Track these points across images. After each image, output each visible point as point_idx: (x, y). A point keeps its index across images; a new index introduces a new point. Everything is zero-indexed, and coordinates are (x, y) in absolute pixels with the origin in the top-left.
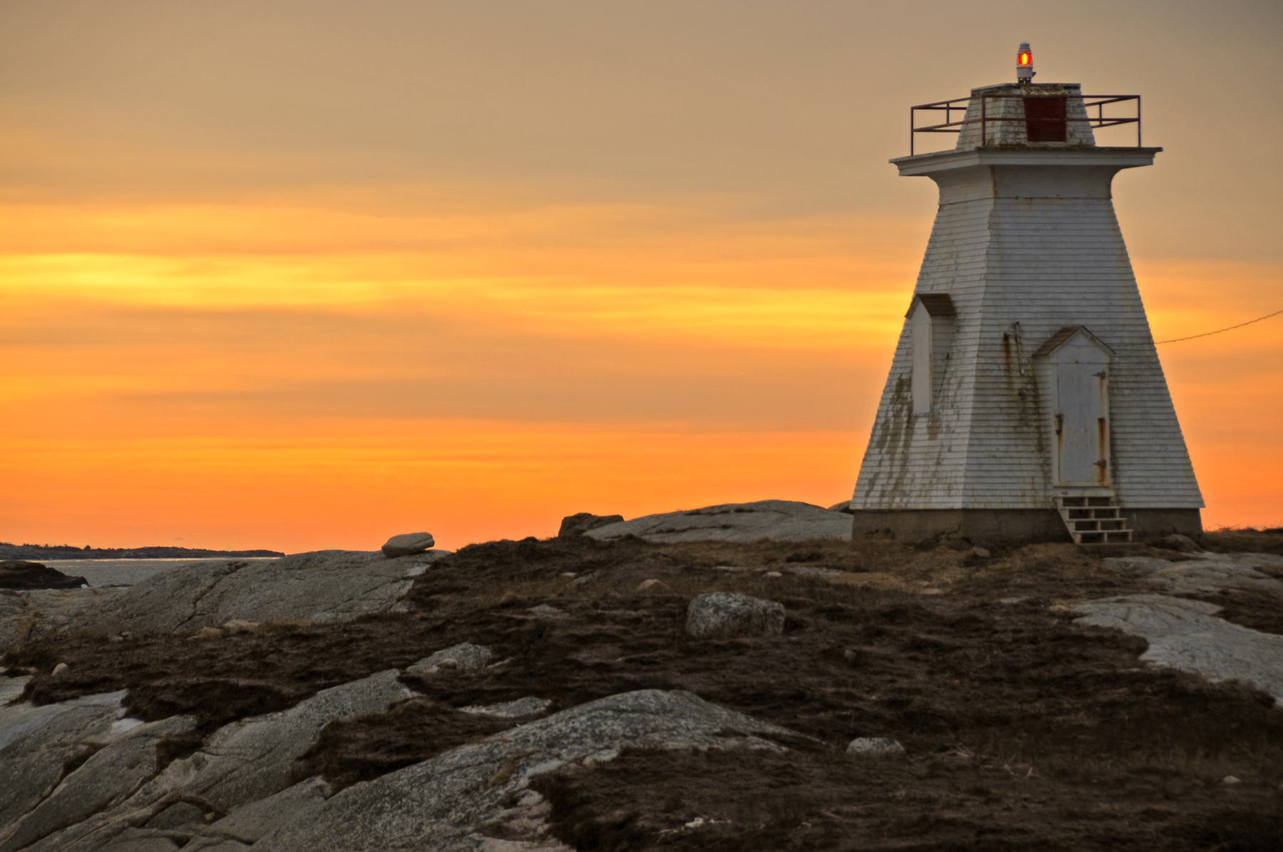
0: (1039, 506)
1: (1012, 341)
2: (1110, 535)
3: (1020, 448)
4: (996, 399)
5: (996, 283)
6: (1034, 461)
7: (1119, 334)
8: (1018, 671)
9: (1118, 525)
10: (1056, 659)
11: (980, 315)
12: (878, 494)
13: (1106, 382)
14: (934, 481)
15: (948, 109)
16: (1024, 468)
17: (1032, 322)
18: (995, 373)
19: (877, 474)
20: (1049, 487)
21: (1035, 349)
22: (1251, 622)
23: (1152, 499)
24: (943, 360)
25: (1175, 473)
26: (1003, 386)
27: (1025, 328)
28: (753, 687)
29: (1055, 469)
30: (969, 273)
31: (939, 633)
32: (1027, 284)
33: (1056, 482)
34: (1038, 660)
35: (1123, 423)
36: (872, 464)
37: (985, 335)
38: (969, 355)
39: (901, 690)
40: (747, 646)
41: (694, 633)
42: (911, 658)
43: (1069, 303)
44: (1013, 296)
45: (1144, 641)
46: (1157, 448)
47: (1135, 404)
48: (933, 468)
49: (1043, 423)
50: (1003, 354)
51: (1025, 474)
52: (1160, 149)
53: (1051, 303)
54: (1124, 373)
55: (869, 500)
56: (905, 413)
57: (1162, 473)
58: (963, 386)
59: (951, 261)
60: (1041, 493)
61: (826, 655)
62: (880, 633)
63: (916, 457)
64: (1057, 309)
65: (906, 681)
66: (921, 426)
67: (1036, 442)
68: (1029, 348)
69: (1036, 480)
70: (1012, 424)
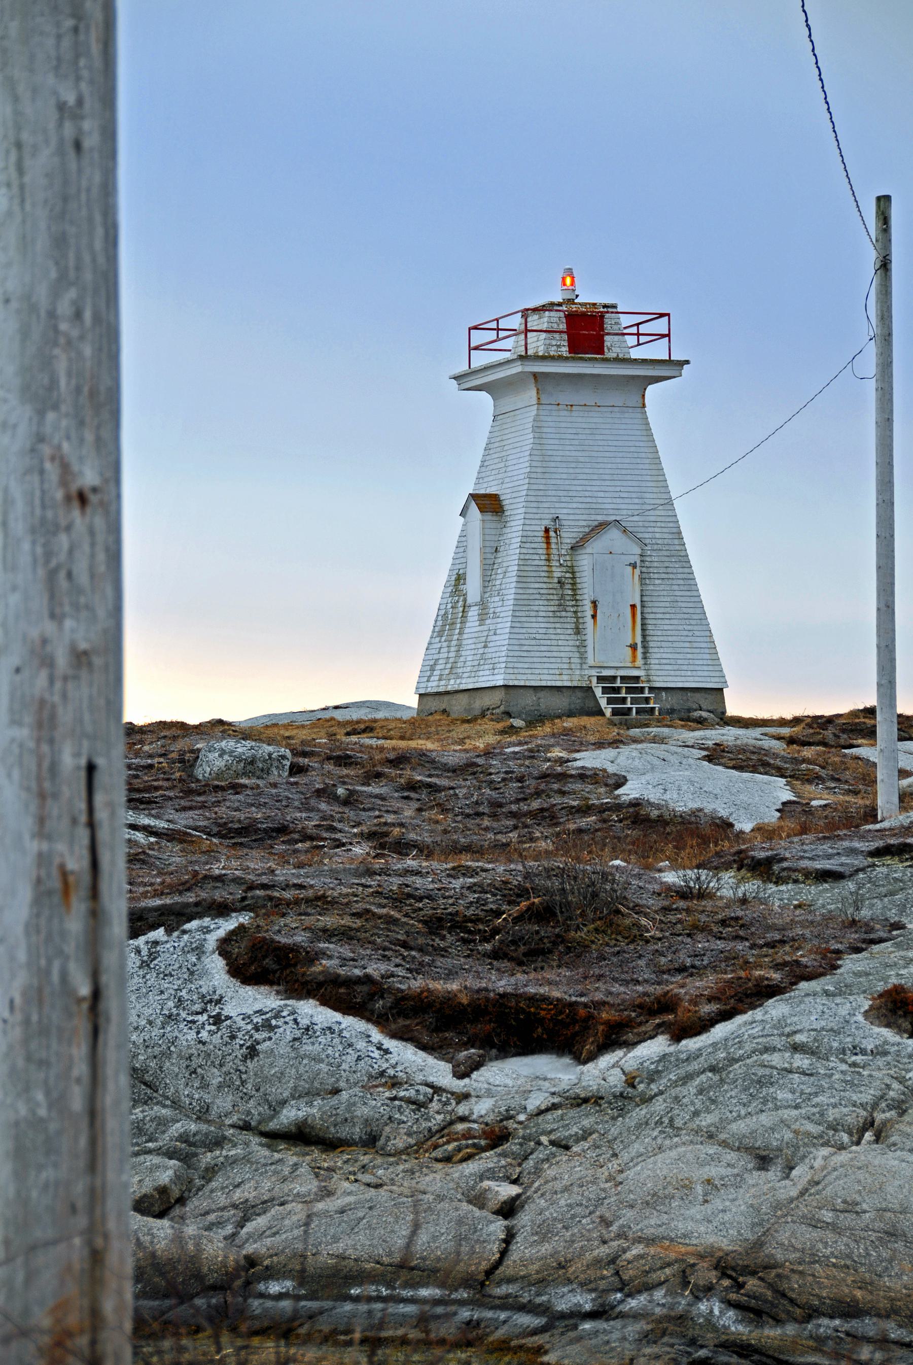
0: (575, 684)
1: (552, 534)
2: (639, 711)
3: (559, 631)
4: (537, 586)
5: (538, 481)
6: (571, 643)
7: (650, 530)
8: (500, 805)
9: (647, 700)
10: (538, 794)
11: (523, 510)
12: (437, 678)
13: (637, 571)
14: (482, 662)
15: (498, 329)
16: (562, 649)
17: (571, 517)
18: (536, 563)
19: (437, 660)
20: (585, 666)
21: (574, 541)
22: (731, 764)
23: (679, 679)
24: (492, 553)
25: (700, 656)
26: (543, 574)
27: (564, 523)
28: (239, 821)
29: (590, 649)
30: (515, 473)
31: (438, 776)
32: (567, 482)
33: (591, 662)
34: (522, 796)
35: (654, 610)
36: (433, 651)
37: (527, 528)
38: (512, 547)
39: (386, 824)
40: (245, 786)
41: (200, 777)
42: (403, 798)
43: (605, 501)
44: (554, 493)
45: (625, 777)
46: (685, 633)
47: (665, 593)
48: (481, 651)
49: (579, 609)
50: (544, 546)
51: (562, 654)
52: (687, 362)
53: (589, 500)
54: (655, 564)
55: (430, 684)
56: (461, 603)
57: (689, 656)
58: (508, 575)
59: (502, 465)
60: (578, 672)
61: (319, 793)
62: (379, 775)
63: (468, 642)
64: (594, 506)
65: (393, 816)
66: (473, 613)
67: (573, 626)
68: (568, 537)
69: (572, 660)
70: (552, 609)
